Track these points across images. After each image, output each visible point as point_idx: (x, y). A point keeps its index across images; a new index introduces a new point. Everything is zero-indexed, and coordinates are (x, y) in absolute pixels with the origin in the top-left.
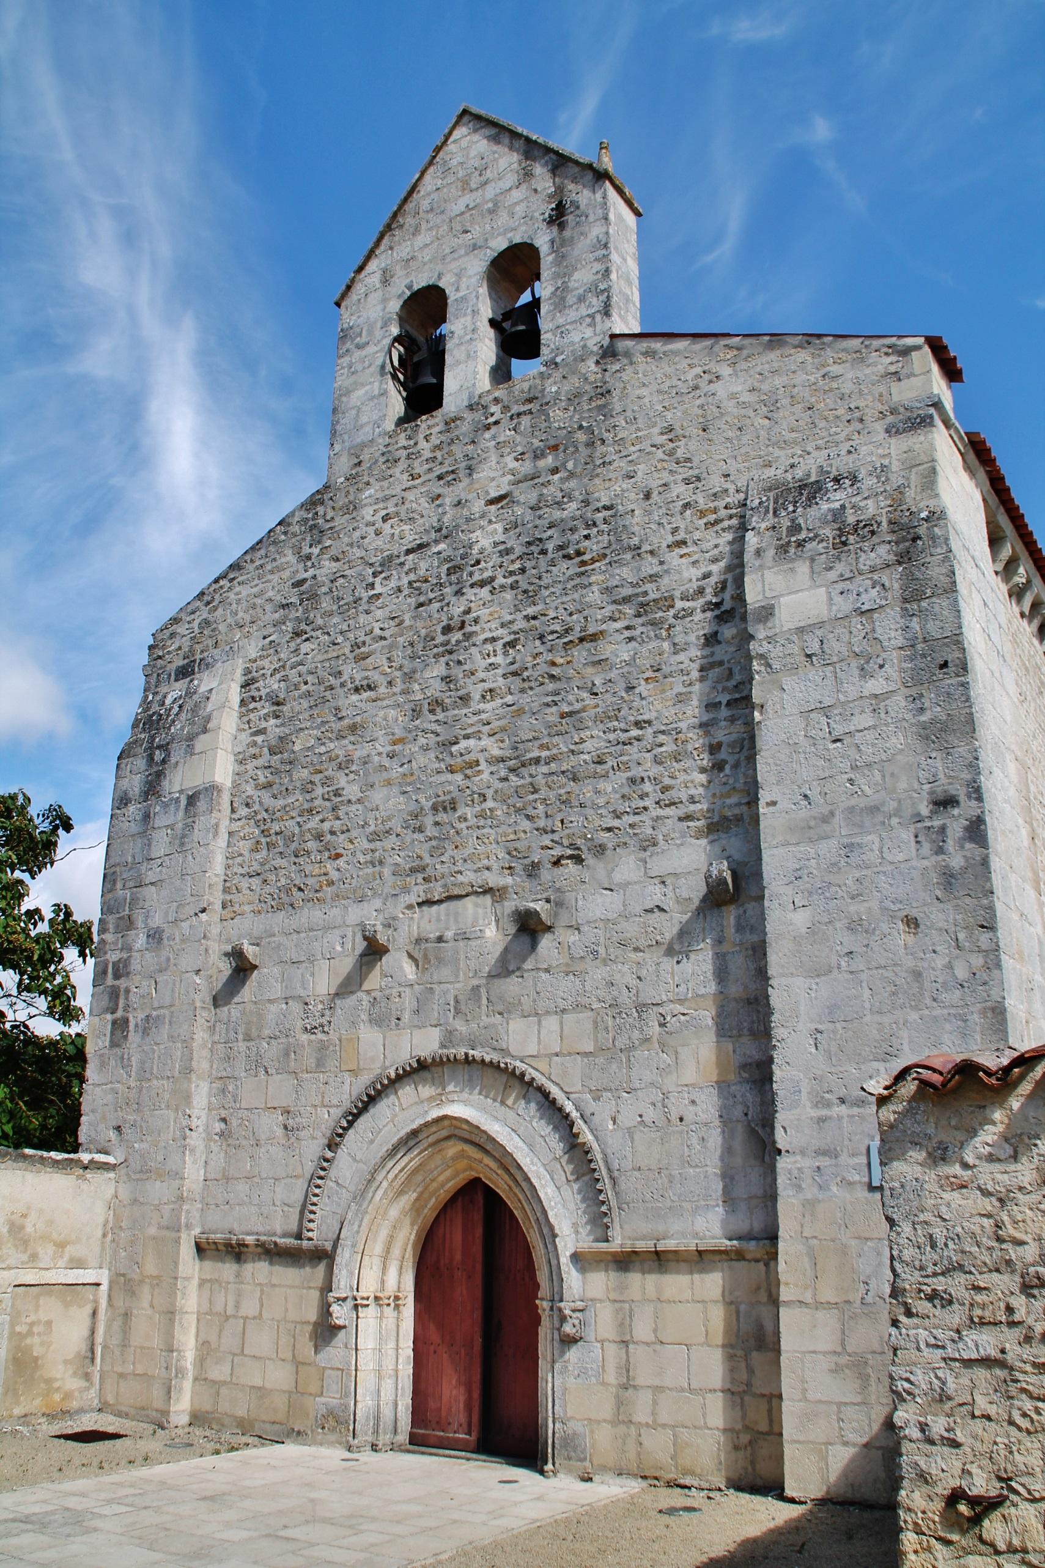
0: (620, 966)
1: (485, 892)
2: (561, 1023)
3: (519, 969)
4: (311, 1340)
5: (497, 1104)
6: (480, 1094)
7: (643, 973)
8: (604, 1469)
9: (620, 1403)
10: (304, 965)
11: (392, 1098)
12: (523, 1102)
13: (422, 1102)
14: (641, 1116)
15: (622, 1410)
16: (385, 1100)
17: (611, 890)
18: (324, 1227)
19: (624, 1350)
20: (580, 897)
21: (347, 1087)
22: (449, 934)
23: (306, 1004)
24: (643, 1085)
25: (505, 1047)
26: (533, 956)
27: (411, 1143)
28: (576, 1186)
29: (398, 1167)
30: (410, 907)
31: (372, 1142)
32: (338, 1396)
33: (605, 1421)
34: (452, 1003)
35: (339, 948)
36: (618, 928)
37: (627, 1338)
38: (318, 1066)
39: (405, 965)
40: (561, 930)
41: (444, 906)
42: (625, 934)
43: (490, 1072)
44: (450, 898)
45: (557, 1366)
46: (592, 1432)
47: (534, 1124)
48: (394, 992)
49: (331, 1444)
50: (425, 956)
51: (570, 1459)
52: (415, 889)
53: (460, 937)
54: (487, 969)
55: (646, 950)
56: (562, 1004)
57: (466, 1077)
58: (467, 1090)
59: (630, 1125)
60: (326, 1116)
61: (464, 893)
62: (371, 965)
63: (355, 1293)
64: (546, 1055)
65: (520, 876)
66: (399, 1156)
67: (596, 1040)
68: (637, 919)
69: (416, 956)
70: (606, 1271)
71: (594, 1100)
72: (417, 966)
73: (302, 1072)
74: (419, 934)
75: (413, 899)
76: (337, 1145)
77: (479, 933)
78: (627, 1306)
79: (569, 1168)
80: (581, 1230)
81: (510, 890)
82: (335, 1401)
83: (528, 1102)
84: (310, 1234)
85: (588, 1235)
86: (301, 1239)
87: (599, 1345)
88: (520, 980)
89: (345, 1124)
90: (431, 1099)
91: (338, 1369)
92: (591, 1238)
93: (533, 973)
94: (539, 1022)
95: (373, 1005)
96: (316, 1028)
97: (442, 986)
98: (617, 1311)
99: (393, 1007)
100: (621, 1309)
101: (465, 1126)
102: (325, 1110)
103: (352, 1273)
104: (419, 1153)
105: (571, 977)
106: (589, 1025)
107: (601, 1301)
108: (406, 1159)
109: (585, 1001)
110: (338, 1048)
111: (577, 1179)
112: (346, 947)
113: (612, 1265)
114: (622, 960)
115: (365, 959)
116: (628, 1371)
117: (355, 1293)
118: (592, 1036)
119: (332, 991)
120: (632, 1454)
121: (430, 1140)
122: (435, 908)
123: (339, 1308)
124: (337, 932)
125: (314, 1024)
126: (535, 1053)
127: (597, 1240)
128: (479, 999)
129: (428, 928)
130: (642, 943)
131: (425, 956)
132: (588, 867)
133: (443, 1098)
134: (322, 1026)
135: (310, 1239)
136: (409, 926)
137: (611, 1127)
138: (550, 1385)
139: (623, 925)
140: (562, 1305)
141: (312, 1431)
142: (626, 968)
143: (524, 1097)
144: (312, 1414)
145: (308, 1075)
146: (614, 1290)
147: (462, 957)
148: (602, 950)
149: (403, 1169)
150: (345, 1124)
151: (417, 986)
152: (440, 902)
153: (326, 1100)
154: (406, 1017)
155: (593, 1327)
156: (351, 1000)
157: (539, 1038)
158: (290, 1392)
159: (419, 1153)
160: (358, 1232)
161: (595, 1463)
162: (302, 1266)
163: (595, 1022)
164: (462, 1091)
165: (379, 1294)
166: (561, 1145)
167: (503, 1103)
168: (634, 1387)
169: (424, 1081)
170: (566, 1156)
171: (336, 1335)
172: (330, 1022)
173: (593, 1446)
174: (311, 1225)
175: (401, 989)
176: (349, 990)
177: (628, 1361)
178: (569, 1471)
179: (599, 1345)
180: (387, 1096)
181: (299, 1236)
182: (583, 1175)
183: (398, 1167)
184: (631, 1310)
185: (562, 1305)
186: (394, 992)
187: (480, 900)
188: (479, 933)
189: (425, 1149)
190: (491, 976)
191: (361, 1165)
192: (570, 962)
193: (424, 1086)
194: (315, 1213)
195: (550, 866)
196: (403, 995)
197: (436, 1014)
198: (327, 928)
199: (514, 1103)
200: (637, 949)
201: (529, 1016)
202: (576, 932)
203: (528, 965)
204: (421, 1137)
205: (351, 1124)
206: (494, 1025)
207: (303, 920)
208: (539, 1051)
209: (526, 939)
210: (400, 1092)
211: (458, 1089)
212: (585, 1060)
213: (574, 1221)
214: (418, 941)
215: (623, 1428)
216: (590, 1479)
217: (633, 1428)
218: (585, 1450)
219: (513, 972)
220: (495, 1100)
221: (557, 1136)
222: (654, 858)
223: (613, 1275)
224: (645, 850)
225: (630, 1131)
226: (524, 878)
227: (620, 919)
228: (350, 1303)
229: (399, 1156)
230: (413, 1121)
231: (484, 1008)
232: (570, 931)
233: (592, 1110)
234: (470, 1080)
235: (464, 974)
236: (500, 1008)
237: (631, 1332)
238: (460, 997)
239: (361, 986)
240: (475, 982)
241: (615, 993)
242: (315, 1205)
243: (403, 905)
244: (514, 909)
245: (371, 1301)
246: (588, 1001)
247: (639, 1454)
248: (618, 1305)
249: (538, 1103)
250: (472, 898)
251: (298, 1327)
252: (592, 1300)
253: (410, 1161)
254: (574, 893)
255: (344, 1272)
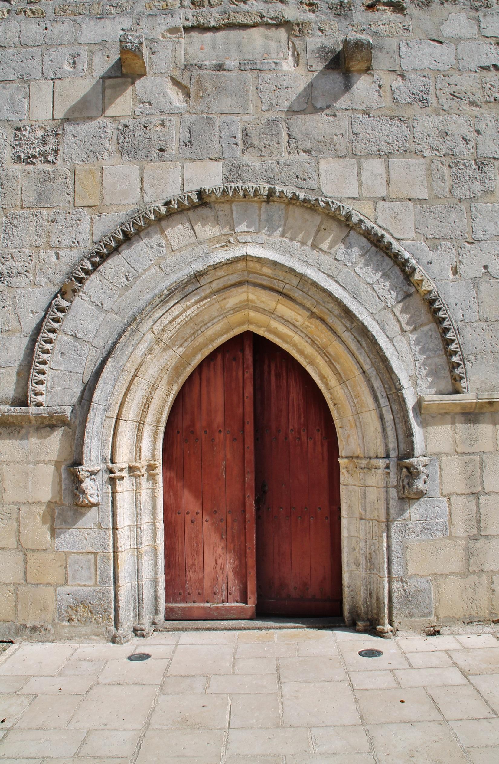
0: (454, 117)
1: (278, 25)
2: (387, 167)
3: (328, 107)
4: (44, 522)
5: (307, 248)
6: (283, 235)
7: (482, 127)
8: (452, 620)
9: (469, 554)
10: (14, 85)
11: (157, 238)
12: (342, 246)
13: (201, 243)
14: (486, 267)
15: (472, 561)
16: (146, 240)
17: (441, 43)
18: (57, 389)
19: (474, 502)
20: (403, 44)
21: (85, 225)
22: (232, 63)
23: (19, 129)
24: (487, 237)
25: (315, 187)
26: (347, 95)
27: (190, 288)
28: (413, 337)
29: (169, 317)
30: (173, 30)
31: (127, 288)
32: (92, 583)
33: (453, 574)
34: (239, 135)
35: (67, 68)
36: (451, 80)
37: (478, 489)
38: (39, 199)
39: (169, 91)
40: (382, 74)
41: (220, 35)
42: (459, 87)
43: (297, 212)
44: (231, 26)
45: (395, 526)
46: (438, 586)
47: (358, 270)
48: (155, 120)
49: (84, 637)
50: (199, 83)
51: (411, 615)
52: (182, 11)
53: (248, 67)
54: (287, 104)
55: (483, 105)
56: (385, 148)
57: (263, 217)
58: (264, 231)
59: (475, 275)
60: (54, 259)
61: (251, 22)
62: (119, 90)
63: (110, 465)
64: (369, 199)
65: (326, 14)
66: (171, 304)
67: (430, 187)
68: (473, 74)
69: (185, 82)
70: (453, 423)
71: (430, 248)
72: (188, 95)
73: (14, 207)
74: (186, 60)
75: (178, 22)
76: (74, 291)
77: (274, 66)
78: (477, 458)
79: (404, 318)
80: (420, 382)
81: (313, 25)
82: (86, 589)
83: (349, 246)
84: (40, 398)
85: (429, 387)
86: (26, 405)
87: (445, 499)
88: (331, 118)
89: (89, 266)
90: (215, 239)
91: (91, 553)
92: (434, 390)
93: (349, 113)
94: (359, 164)
95: (123, 133)
96: (34, 157)
97: (224, 117)
98: (467, 464)
99: (154, 136)
100: (470, 461)
101: (266, 270)
102: (52, 253)
103: (104, 442)
104: (197, 302)
105: (396, 122)
106: (422, 173)
107: (447, 454)
108: (179, 308)
109: (412, 147)
110: (70, 181)
111: (415, 329)
112: (79, 67)
113: (458, 418)
114: (456, 111)
115: (108, 82)
116: (479, 522)
117: (110, 465)
118: (425, 184)
119: (59, 115)
120: (484, 603)
121: (214, 286)
122: (209, 35)
123: (92, 483)
124: (65, 50)
125: (32, 152)
126: (356, 196)
127: (440, 393)
128: (278, 134)
129: (200, 55)
130: (478, 97)
131: (199, 83)
132: (411, 16)
133: (231, 239)
134: (44, 155)
135: (39, 404)
136: (174, 50)
137: (451, 276)
138: (385, 545)
139: (456, 78)
140: (414, 460)
141: (54, 625)
142: (461, 120)
143: (343, 241)
144: (52, 607)
145: (25, 211)
146: (463, 442)
147: (252, 89)
148: (432, 99)
149: (174, 319)
150: (89, 266)
151: (187, 116)
152: (216, 29)
153: (53, 240)
154: (173, 148)
155: (437, 482)
156: (90, 127)
157: (360, 180)
158: (16, 585)
159: (197, 302)
160: (112, 393)
161: (441, 616)
162: (26, 437)
163: (429, 170)
164: (257, 232)
165: (134, 464)
166: (394, 294)
167: (314, 246)
168: (486, 537)
169: (204, 220)
170: (401, 305)
171: (83, 515)
172: (56, 152)
173: (439, 600)
174: (41, 388)
175: (164, 117)
176: (86, 114)
177: (478, 512)
178: (412, 628)
179: (445, 499)
180: (148, 235)
181: (22, 401)
182: (422, 325)
183: (169, 317)
184: (482, 462)
185: (414, 460)
186: (155, 120)
187: (272, 32)
188: (274, 66)
189: (205, 298)
190: (291, 111)
191: (111, 316)
192: (394, 106)
193: (204, 225)
194: (44, 373)
195: (363, 8)
196: (167, 123)
197: (218, 148)
198: (48, 45)
199: (330, 247)
200: (472, 103)
201: (345, 156)
202: (400, 78)
203: (342, 103)
204: (203, 281)
205: (95, 266)
206: (298, 163)
207: (10, 34)
208: (360, 193)
209: (336, 78)
210: (168, 231)
211: (252, 230)
212: (419, 207)
213: (412, 373)
214: (188, 67)
215: (474, 578)
216: (437, 633)
217: (484, 577)
218: (429, 604)
219: (322, 109)
220: (303, 243)
221: (388, 284)
222: (489, 18)
223: (460, 427)
224: (477, 10)
225: (475, 283)
226: (331, 16)
227: (452, 71)
228: (104, 476)
229: (171, 304)
230: (188, 264)
231: (284, 144)
232: (392, 76)
233: (429, 259)
234: (269, 220)
235: (256, 107)
236: (307, 145)
237: (482, 483)
238: (251, 131)
239: (103, 111)
240: (271, 116)
241: (451, 144)
242: (44, 363)
243: (164, 27)
244: (319, 45)
245: (125, 474)
246: (419, 148)
247: (491, 600)
248: (466, 458)
249: (362, 248)
250: (262, 30)
251: (23, 508)
252: (436, 454)
253: (185, 311)
254: (395, 40)
255: (95, 441)
